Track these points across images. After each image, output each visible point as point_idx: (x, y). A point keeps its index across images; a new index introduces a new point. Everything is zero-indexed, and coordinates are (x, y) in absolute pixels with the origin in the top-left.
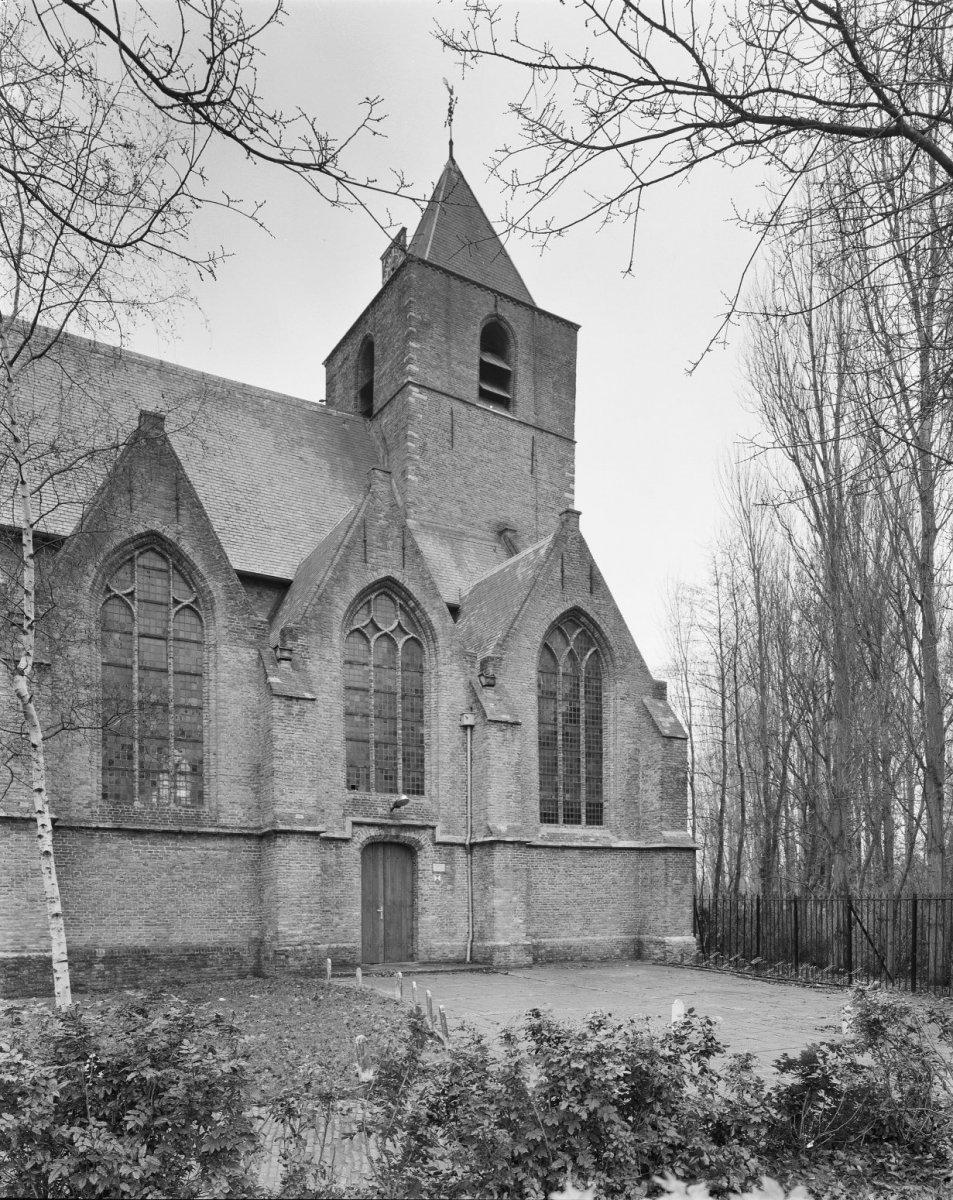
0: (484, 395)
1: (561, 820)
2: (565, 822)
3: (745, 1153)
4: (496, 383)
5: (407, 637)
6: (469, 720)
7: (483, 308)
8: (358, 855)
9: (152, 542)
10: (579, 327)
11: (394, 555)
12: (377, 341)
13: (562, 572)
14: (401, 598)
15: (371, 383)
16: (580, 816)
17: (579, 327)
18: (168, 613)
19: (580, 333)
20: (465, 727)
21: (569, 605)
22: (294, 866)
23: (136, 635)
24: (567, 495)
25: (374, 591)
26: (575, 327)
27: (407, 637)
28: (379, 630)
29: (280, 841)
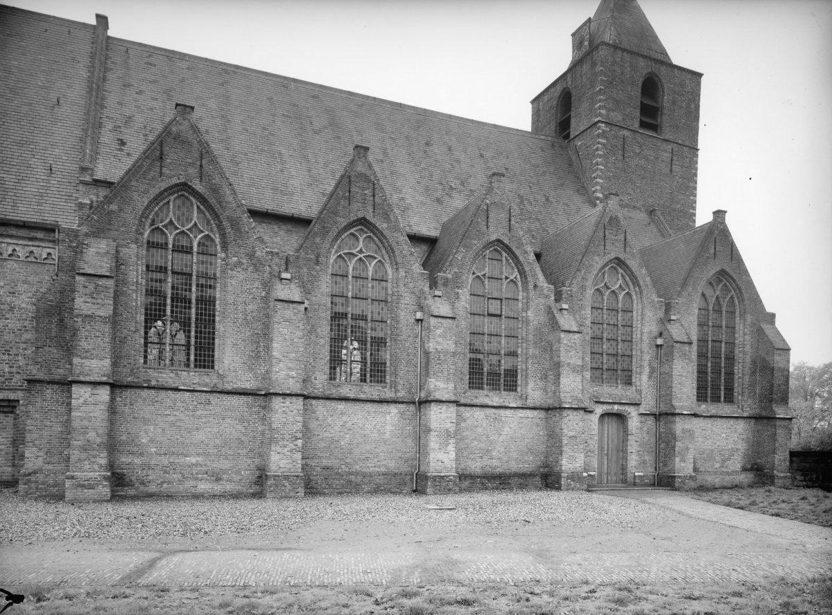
0: (643, 125)
1: (709, 399)
2: (725, 401)
3: (56, 591)
4: (650, 116)
5: (376, 260)
6: (419, 315)
7: (644, 67)
8: (597, 420)
9: (363, 222)
10: (702, 75)
11: (620, 245)
12: (574, 93)
13: (715, 248)
14: (623, 269)
15: (569, 119)
16: (720, 397)
17: (702, 75)
18: (502, 284)
19: (703, 80)
20: (418, 320)
21: (718, 269)
22: (571, 424)
23: (370, 278)
24: (692, 198)
25: (354, 227)
26: (700, 75)
27: (376, 260)
28: (609, 288)
29: (433, 404)
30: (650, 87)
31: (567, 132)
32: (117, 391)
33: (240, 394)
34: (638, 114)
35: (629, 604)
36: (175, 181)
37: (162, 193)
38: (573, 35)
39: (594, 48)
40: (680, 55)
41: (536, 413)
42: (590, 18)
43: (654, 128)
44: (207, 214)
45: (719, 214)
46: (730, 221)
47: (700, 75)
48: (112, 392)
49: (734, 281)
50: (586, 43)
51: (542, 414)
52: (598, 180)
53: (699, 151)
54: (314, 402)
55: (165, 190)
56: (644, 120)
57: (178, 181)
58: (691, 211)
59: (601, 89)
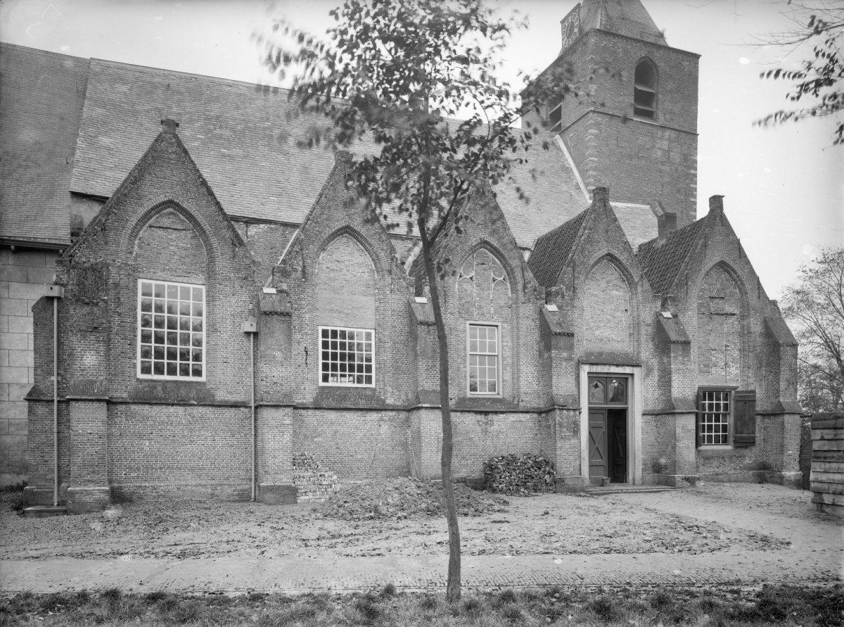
0: (638, 112)
4: (644, 104)
7: (640, 53)
26: (697, 57)
30: (645, 72)
31: (559, 123)
32: (112, 407)
33: (231, 406)
34: (632, 101)
35: (817, 267)
36: (162, 199)
37: (149, 212)
38: (562, 22)
39: (583, 35)
40: (674, 40)
41: (528, 416)
42: (579, 4)
43: (649, 115)
44: (180, 215)
45: (716, 201)
46: (728, 211)
47: (697, 57)
48: (111, 415)
49: (735, 273)
50: (576, 30)
51: (535, 416)
52: (593, 158)
53: (698, 137)
54: (303, 412)
55: (153, 209)
56: (640, 88)
57: (166, 199)
58: (692, 171)
59: (592, 58)
